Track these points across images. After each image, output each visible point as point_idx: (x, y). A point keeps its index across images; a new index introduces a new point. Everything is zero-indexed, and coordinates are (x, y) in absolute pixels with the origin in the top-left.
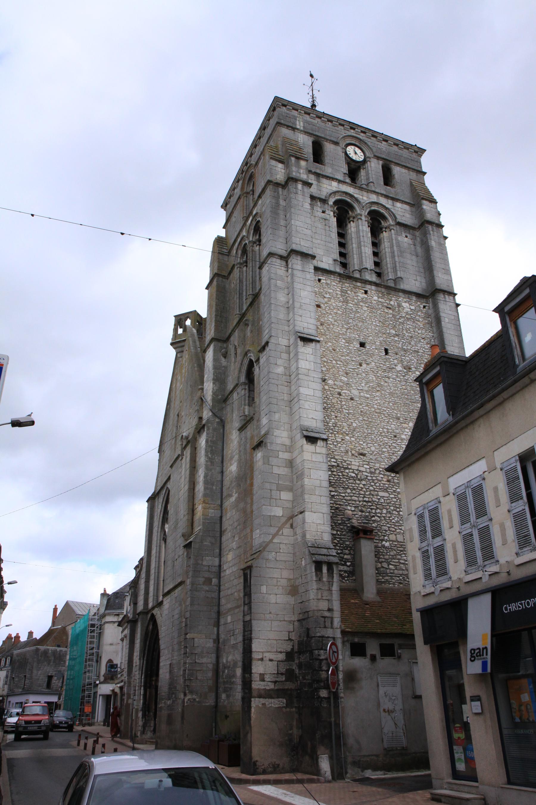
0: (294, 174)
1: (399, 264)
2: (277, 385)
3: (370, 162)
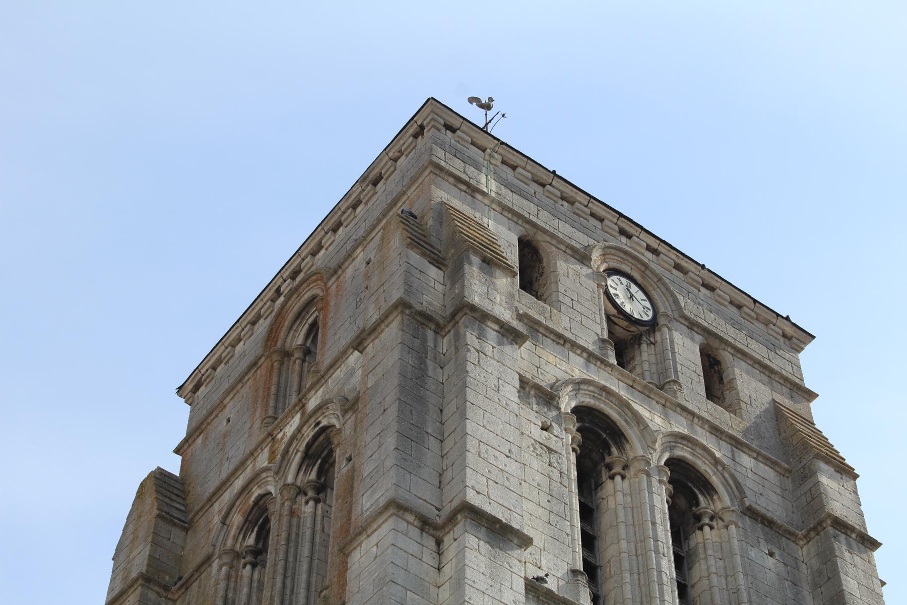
3: (669, 329)
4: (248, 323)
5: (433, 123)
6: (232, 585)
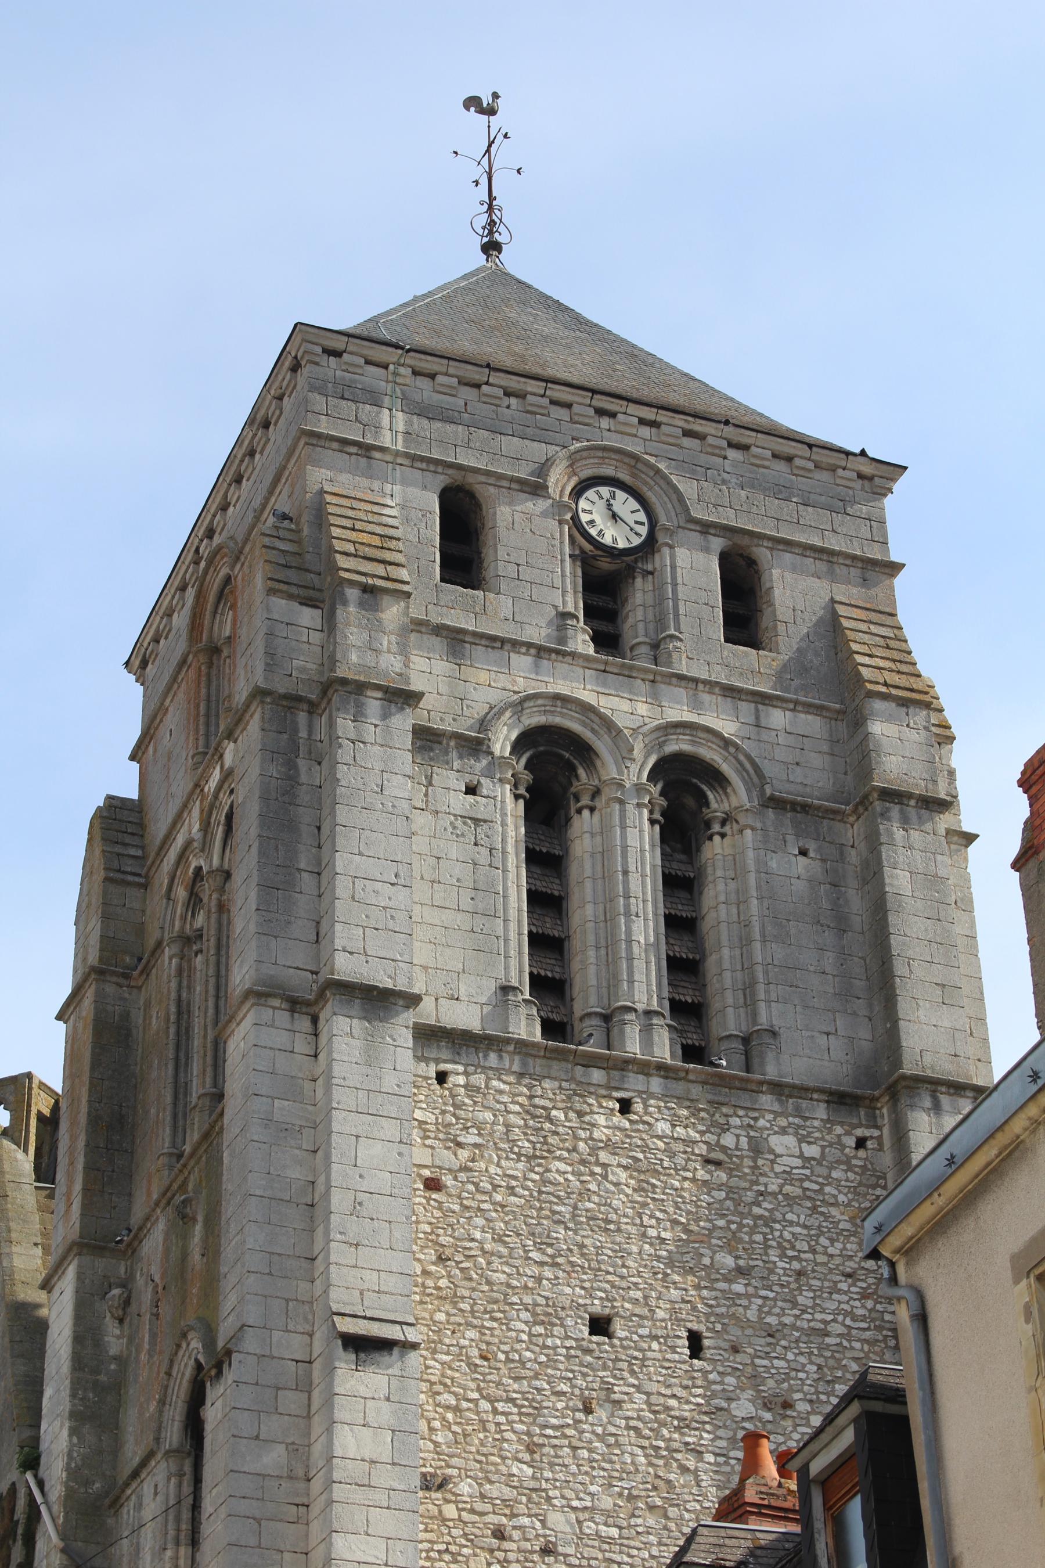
0: (354, 658)
1: (766, 972)
2: (259, 1521)
3: (671, 547)
4: (177, 589)
5: (307, 357)
6: (185, 983)
